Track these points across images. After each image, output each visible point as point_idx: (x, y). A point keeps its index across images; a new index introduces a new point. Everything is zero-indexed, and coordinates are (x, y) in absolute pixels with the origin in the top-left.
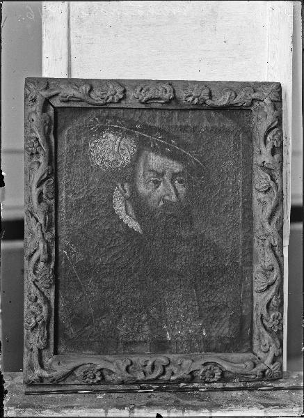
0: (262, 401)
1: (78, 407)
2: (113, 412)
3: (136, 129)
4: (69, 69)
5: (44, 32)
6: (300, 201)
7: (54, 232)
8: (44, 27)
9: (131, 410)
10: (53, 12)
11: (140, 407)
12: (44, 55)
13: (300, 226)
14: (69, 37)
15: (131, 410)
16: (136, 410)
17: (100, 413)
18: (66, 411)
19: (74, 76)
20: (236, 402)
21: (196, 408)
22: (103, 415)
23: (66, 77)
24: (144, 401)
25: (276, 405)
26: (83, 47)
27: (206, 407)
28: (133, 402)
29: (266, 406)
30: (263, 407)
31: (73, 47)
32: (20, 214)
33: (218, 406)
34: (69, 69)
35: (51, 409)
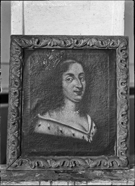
0: (110, 177)
1: (27, 181)
2: (43, 183)
3: (49, 57)
4: (23, 32)
5: (12, 10)
6: (133, 85)
7: (21, 88)
8: (12, 8)
9: (51, 182)
10: (16, 6)
11: (55, 180)
12: (12, 21)
13: (133, 97)
14: (23, 13)
15: (51, 182)
16: (53, 182)
17: (37, 183)
18: (22, 182)
19: (26, 34)
20: (99, 178)
21: (80, 181)
22: (38, 184)
23: (21, 34)
24: (57, 178)
25: (117, 179)
26: (30, 20)
27: (84, 180)
28: (52, 178)
29: (112, 180)
30: (110, 180)
31: (25, 16)
32: (7, 91)
33: (90, 180)
34: (23, 32)
35: (15, 182)
